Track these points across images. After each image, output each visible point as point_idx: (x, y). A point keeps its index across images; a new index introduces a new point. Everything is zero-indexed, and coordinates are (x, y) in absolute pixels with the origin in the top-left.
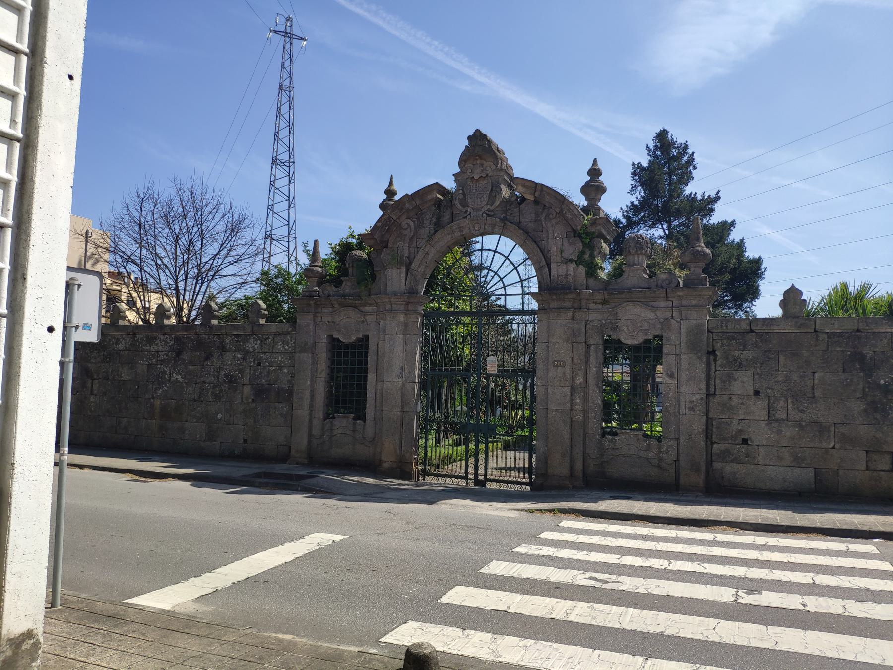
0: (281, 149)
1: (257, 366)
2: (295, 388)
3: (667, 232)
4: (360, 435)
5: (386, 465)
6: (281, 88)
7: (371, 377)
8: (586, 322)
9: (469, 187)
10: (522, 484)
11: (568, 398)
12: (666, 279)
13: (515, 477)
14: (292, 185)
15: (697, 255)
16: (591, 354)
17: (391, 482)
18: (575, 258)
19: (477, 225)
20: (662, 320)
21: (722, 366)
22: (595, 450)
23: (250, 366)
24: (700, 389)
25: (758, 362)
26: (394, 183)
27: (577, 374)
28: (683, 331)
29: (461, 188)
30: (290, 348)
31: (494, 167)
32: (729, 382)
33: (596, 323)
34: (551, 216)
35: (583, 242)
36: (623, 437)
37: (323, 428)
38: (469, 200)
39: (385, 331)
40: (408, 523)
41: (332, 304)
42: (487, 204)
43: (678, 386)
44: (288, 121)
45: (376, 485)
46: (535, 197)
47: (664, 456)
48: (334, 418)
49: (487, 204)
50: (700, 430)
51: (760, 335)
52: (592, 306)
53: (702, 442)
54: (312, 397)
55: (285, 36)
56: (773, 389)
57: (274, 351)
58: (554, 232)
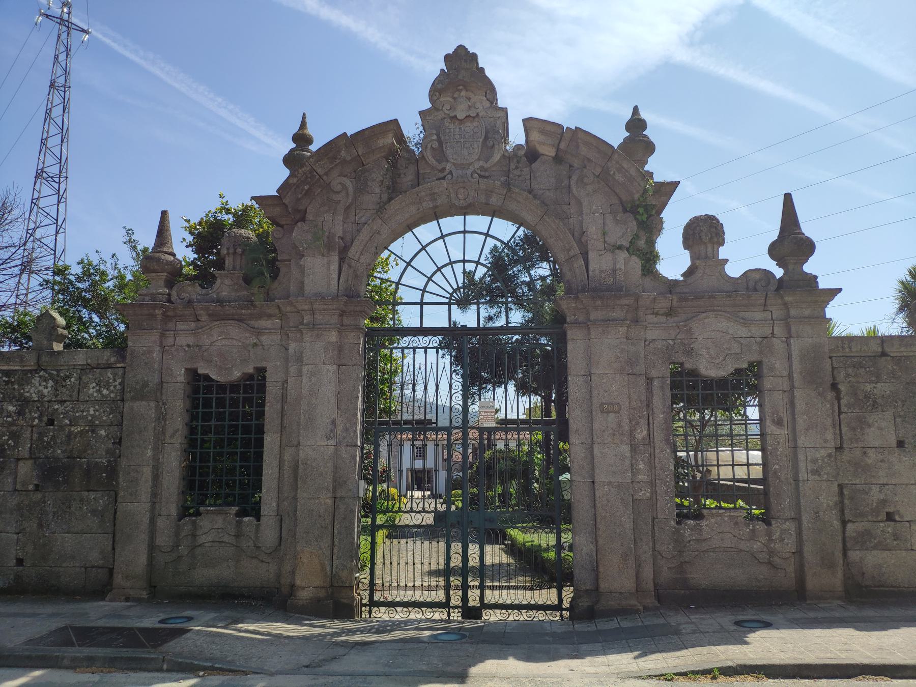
0: (50, 160)
1: (47, 425)
2: (123, 463)
4: (251, 543)
5: (304, 595)
6: (52, 85)
7: (271, 441)
9: (448, 131)
11: (628, 462)
12: (760, 280)
14: (62, 206)
16: (654, 392)
17: (323, 626)
18: (626, 244)
19: (462, 190)
20: (759, 340)
21: (849, 406)
22: (669, 544)
23: (33, 426)
24: (826, 441)
27: (638, 423)
30: (112, 392)
32: (861, 429)
33: (659, 345)
36: (713, 521)
37: (177, 534)
42: (479, 159)
44: (61, 127)
45: (305, 638)
46: (558, 149)
47: (777, 546)
48: (198, 514)
49: (479, 159)
50: (831, 503)
51: (898, 360)
52: (651, 318)
55: (60, 24)
57: (82, 398)
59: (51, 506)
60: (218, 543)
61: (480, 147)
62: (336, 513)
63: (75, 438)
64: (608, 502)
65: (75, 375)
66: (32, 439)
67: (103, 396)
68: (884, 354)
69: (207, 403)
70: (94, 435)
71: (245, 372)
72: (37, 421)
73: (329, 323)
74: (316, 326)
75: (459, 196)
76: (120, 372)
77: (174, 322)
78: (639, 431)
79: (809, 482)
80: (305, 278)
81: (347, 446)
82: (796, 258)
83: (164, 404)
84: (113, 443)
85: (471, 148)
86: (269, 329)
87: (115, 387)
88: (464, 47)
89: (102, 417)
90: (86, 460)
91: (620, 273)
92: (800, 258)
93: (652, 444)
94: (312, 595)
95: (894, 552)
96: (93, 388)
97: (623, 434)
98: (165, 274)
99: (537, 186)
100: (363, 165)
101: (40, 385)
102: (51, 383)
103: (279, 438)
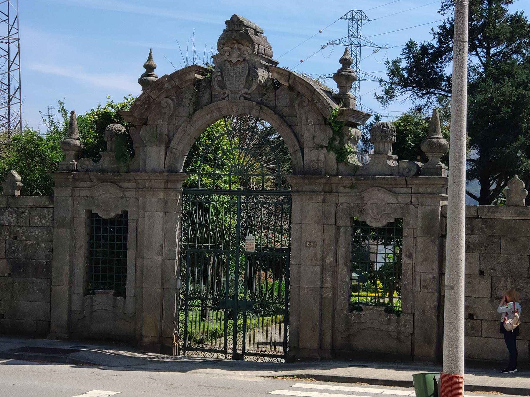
2: (54, 263)
3: (484, 60)
5: (147, 340)
7: (131, 253)
8: (337, 204)
10: (277, 356)
11: (318, 276)
13: (271, 351)
15: (433, 146)
16: (341, 235)
17: (151, 355)
19: (235, 107)
20: (402, 205)
23: (6, 240)
24: (433, 269)
25: (483, 245)
26: (153, 57)
27: (328, 254)
28: (420, 215)
29: (219, 70)
30: (47, 222)
31: (250, 52)
33: (345, 206)
34: (304, 104)
35: (333, 130)
36: (367, 312)
37: (83, 303)
38: (227, 83)
39: (144, 208)
40: (167, 385)
41: (91, 179)
42: (245, 88)
43: (414, 266)
47: (402, 329)
48: (94, 293)
49: (245, 88)
50: (432, 306)
51: (485, 221)
52: (341, 189)
53: (434, 317)
54: (72, 271)
56: (495, 270)
57: (31, 225)
58: (307, 118)
59: (17, 286)
60: (104, 310)
61: (245, 80)
62: (164, 297)
63: (29, 247)
64: (307, 298)
65: (27, 211)
66: (6, 248)
67: (43, 224)
68: (478, 217)
69: (98, 229)
70: (39, 246)
71: (117, 213)
72: (8, 237)
73: (159, 187)
74: (152, 189)
75: (233, 110)
76: (51, 210)
77: (79, 182)
78: (328, 258)
79: (421, 293)
80: (147, 159)
81: (170, 259)
82: (432, 153)
83: (75, 230)
84: (49, 251)
85: (240, 81)
86: (129, 188)
87: (49, 219)
88: (237, 16)
89: (42, 236)
90: (35, 260)
91: (321, 163)
92: (434, 153)
93: (337, 266)
94: (150, 341)
95: (471, 337)
96: (37, 219)
97: (317, 260)
98: (74, 152)
99: (279, 104)
100: (180, 89)
101: (9, 216)
102: (14, 215)
103: (135, 253)
